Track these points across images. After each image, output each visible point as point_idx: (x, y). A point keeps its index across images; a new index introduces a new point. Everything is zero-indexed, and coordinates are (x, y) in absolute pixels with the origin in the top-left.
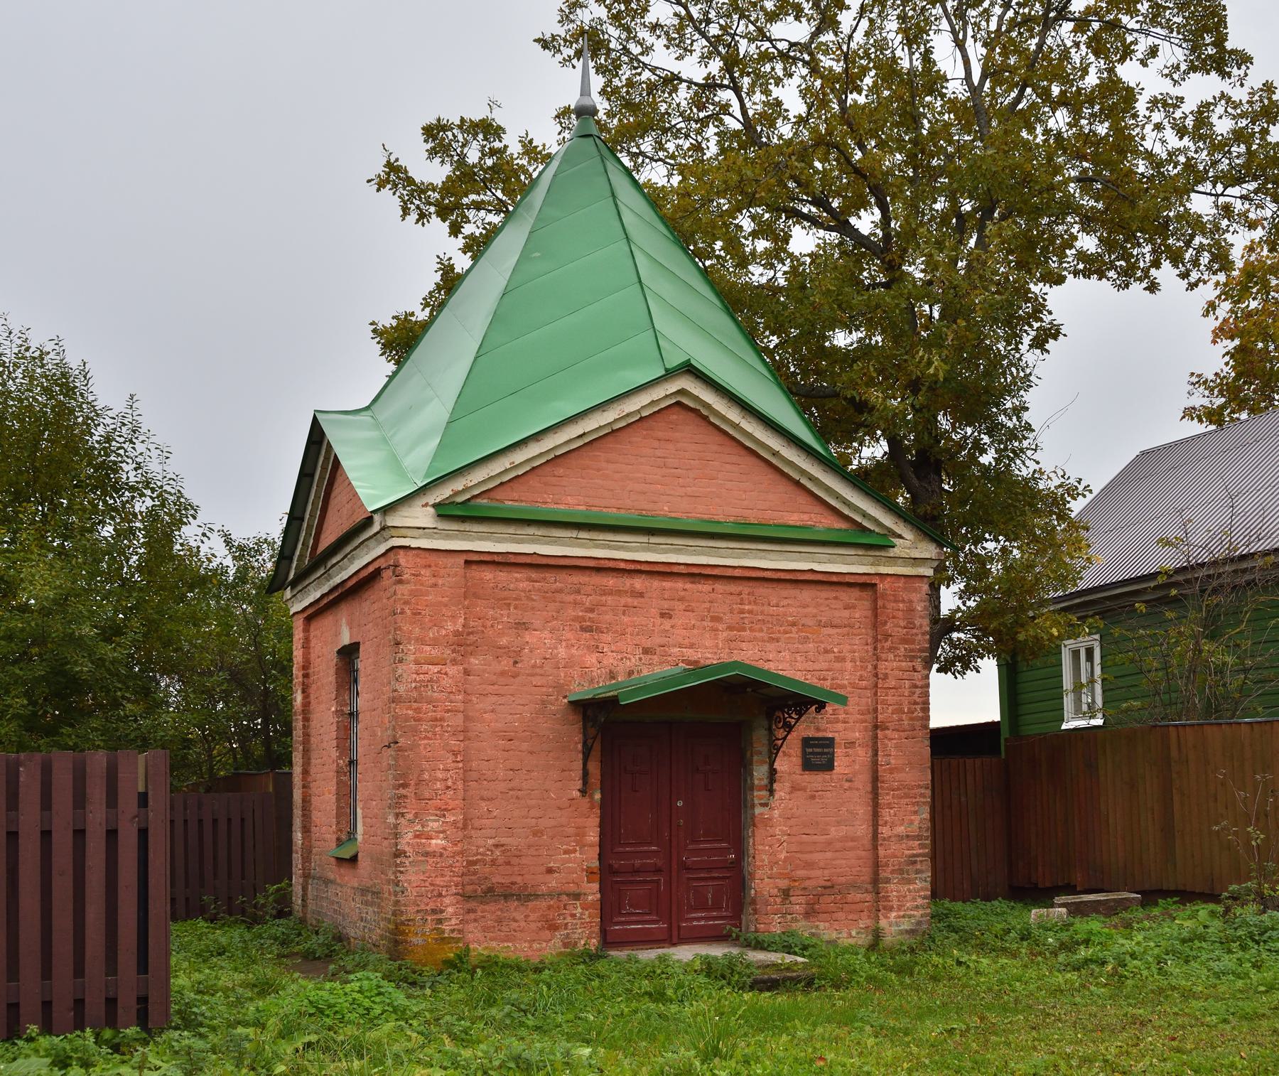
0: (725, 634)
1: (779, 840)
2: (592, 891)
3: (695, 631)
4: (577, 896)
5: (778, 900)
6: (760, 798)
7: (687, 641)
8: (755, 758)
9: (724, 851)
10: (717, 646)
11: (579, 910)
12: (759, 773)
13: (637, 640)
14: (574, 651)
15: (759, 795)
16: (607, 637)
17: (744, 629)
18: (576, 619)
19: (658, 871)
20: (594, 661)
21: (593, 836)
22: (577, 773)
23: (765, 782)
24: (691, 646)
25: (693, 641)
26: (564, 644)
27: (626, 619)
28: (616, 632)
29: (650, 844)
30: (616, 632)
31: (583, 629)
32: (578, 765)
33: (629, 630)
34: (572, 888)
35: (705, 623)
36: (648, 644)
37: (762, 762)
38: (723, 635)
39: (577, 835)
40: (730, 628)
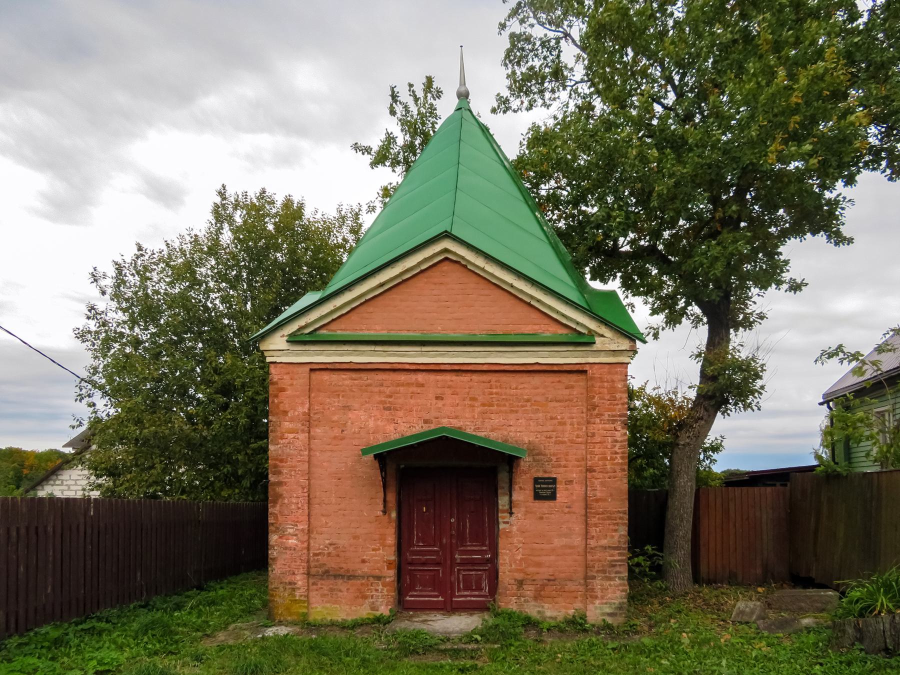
0: (479, 409)
1: (516, 547)
2: (391, 575)
3: (459, 408)
4: (379, 578)
5: (515, 587)
6: (503, 518)
8: (499, 491)
10: (474, 417)
11: (381, 587)
12: (503, 501)
14: (379, 423)
15: (503, 517)
16: (401, 413)
17: (493, 405)
19: (438, 564)
20: (392, 429)
21: (391, 540)
22: (380, 502)
23: (507, 507)
24: (456, 417)
29: (434, 546)
33: (415, 409)
36: (427, 417)
37: (505, 494)
39: (380, 539)
40: (483, 405)
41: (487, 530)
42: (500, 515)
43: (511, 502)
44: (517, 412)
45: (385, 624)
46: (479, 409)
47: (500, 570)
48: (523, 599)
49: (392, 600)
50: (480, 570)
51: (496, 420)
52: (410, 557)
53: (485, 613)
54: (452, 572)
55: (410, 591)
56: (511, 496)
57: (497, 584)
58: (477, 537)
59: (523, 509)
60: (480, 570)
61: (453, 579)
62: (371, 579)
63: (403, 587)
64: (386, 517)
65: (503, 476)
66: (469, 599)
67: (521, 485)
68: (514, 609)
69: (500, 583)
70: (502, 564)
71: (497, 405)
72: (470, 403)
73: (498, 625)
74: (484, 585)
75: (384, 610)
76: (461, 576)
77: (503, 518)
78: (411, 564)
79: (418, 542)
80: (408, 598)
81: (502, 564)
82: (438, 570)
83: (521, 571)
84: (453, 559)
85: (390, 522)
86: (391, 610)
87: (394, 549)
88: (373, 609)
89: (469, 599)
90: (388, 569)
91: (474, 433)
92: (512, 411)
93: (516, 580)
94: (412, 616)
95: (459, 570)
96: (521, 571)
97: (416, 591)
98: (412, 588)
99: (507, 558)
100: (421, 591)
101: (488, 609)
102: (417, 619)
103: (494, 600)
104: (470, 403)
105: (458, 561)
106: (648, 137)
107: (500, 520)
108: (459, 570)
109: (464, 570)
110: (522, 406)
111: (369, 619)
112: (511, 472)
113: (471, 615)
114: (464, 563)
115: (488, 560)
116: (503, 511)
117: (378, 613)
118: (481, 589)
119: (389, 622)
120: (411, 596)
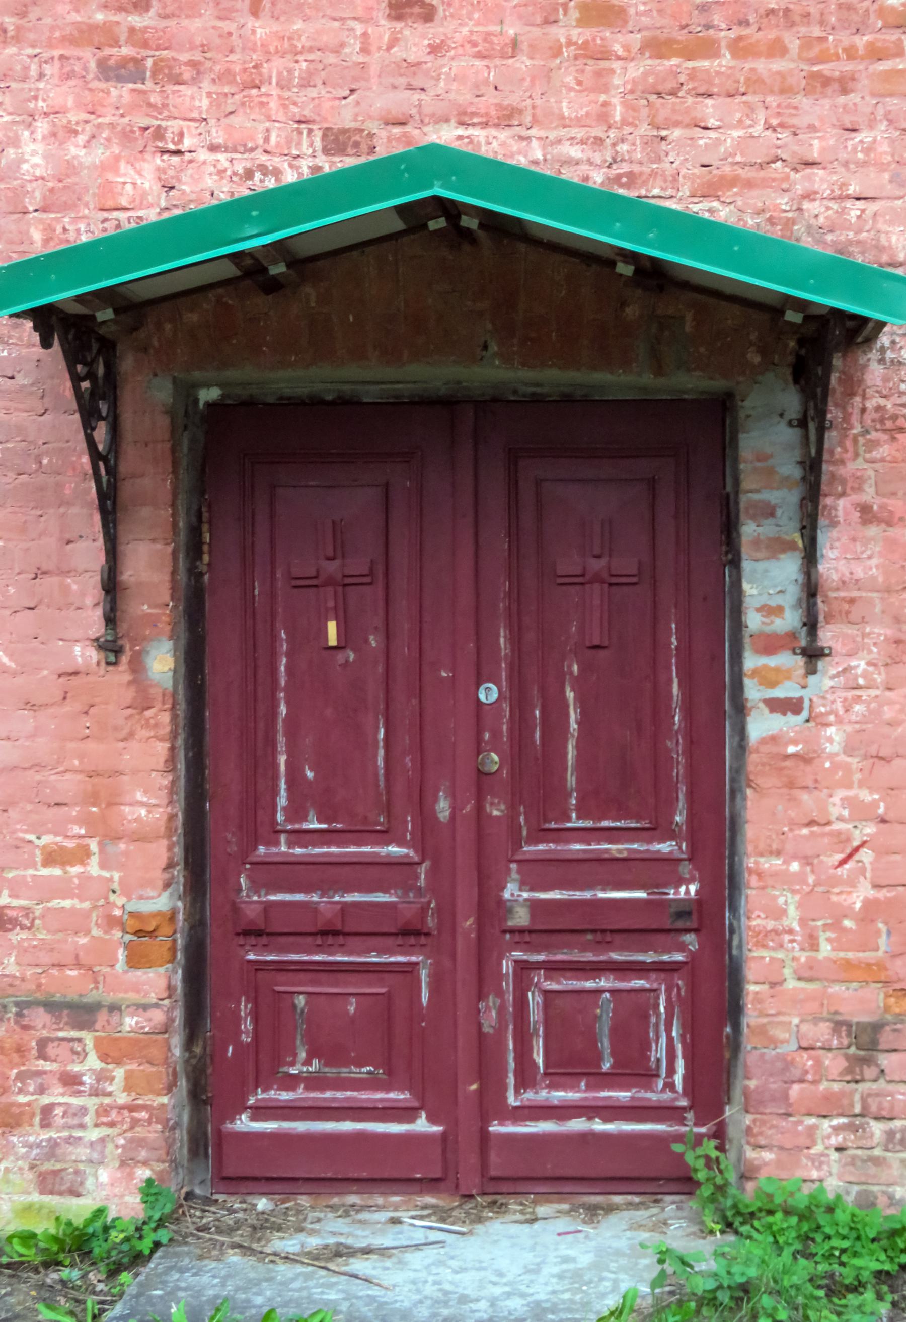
0: (635, 70)
1: (841, 839)
2: (149, 992)
3: (523, 63)
4: (82, 1014)
5: (834, 1063)
6: (769, 679)
7: (491, 99)
8: (749, 530)
9: (661, 871)
10: (603, 117)
11: (93, 1062)
12: (767, 586)
13: (305, 101)
14: (75, 150)
15: (766, 673)
16: (197, 98)
17: (709, 49)
18: (87, 35)
19: (410, 933)
20: (148, 183)
21: (150, 802)
22: (87, 589)
23: (790, 620)
24: (507, 117)
25: (513, 99)
26: (42, 126)
27: (262, 29)
28: (227, 76)
29: (385, 836)
30: (227, 76)
31: (111, 71)
32: (90, 554)
33: (274, 68)
34: (72, 983)
35: (559, 33)
36: (345, 117)
37: (777, 547)
38: (627, 74)
39: (93, 798)
40: (658, 47)
41: (676, 748)
42: (751, 661)
43: (811, 590)
44: (845, 85)
45: (113, 1273)
46: (635, 70)
47: (751, 972)
48: (877, 1129)
49: (153, 1132)
50: (640, 969)
51: (730, 132)
52: (253, 898)
53: (670, 1205)
54: (484, 981)
55: (261, 1081)
56: (811, 557)
57: (735, 1045)
58: (625, 787)
59: (880, 631)
60: (640, 969)
61: (490, 1020)
62: (40, 1018)
63: (211, 1081)
64: (121, 675)
65: (766, 445)
66: (577, 1125)
67: (868, 495)
68: (833, 1185)
69: (748, 1042)
70: (764, 938)
71: (740, 49)
72: (579, 35)
73: (745, 1290)
74: (659, 1051)
75: (112, 1191)
76: (534, 1000)
77: (769, 679)
78: (254, 933)
79: (296, 812)
80: (244, 1123)
81: (764, 938)
82: (413, 967)
83: (871, 973)
84: (490, 909)
85: (143, 703)
86: (150, 1191)
87: (161, 852)
88: (48, 1182)
89: (577, 1125)
90: (136, 960)
91: (700, 208)
92: (820, 84)
93: (838, 1025)
94: (264, 1226)
95: (523, 967)
96: (871, 973)
97: (291, 1082)
98: (264, 1063)
99: (789, 902)
100: (315, 1082)
101: (685, 1183)
102: (290, 1244)
103: (719, 1134)
104: (579, 35)
105: (521, 918)
106: (99, 411)
107: (753, 692)
108: (523, 967)
109: (553, 969)
110: (876, 54)
111: (28, 1238)
112: (813, 422)
113: (593, 1213)
114: (548, 927)
115: (684, 911)
116: (770, 644)
117: (77, 1210)
118: (644, 1075)
119: (138, 1259)
120: (261, 1112)
